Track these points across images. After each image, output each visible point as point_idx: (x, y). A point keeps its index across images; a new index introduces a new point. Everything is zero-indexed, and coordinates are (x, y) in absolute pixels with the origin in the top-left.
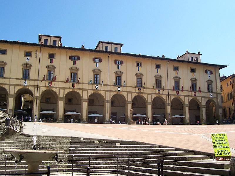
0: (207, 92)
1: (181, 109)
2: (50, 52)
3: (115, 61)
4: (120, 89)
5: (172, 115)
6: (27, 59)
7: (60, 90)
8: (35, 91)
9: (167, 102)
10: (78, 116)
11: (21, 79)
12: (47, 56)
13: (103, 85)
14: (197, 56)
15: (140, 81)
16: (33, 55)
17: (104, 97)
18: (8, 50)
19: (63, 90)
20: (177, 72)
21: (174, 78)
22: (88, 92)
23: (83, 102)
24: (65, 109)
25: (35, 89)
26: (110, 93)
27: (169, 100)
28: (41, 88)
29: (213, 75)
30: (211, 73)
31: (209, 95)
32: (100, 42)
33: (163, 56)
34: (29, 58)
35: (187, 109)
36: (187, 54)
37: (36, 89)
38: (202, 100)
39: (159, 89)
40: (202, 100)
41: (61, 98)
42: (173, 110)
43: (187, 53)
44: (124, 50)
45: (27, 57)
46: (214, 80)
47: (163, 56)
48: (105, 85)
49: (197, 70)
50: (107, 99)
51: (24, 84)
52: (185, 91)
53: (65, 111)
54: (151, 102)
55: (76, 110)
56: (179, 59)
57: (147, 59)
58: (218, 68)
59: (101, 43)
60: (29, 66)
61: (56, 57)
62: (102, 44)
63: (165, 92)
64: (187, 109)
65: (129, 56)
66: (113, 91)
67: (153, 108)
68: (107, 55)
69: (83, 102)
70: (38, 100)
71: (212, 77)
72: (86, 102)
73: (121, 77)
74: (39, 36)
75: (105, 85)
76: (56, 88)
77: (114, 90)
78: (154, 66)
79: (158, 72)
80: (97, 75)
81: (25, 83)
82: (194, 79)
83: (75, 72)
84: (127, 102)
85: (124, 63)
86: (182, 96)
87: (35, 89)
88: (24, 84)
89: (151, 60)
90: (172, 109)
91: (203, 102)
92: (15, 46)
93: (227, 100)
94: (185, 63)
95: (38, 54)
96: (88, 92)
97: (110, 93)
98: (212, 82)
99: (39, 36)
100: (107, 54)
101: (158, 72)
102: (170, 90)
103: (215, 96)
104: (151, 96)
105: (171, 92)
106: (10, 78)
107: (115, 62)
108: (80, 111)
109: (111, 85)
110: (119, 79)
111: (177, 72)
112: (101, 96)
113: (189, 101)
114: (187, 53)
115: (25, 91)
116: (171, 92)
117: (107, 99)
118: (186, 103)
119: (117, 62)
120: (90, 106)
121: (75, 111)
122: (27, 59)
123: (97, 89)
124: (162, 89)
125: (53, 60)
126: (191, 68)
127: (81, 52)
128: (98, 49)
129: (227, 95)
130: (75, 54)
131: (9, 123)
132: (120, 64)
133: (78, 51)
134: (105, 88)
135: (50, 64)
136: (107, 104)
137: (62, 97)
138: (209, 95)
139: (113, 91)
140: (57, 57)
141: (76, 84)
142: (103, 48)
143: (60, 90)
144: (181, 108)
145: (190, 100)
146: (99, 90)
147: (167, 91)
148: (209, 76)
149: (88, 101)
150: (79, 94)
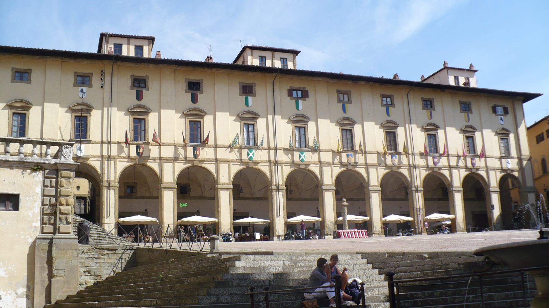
3: (288, 90)
4: (304, 157)
5: (428, 213)
6: (82, 91)
10: (314, 224)
12: (129, 82)
14: (467, 74)
15: (349, 136)
16: (96, 81)
18: (94, 75)
20: (431, 112)
24: (234, 210)
26: (282, 167)
29: (510, 117)
30: (506, 112)
32: (245, 48)
33: (396, 76)
34: (85, 89)
35: (458, 199)
36: (446, 70)
40: (368, 173)
43: (446, 68)
44: (302, 63)
45: (80, 88)
53: (237, 216)
54: (330, 183)
55: (198, 211)
56: (426, 82)
57: (363, 83)
59: (248, 51)
60: (87, 110)
61: (150, 84)
62: (252, 52)
64: (458, 199)
65: (321, 79)
67: (288, 198)
68: (270, 77)
72: (227, 189)
73: (304, 127)
74: (102, 36)
79: (388, 114)
84: (219, 186)
85: (311, 94)
90: (426, 199)
92: (50, 61)
93: (541, 174)
95: (107, 79)
97: (282, 167)
99: (102, 36)
107: (290, 94)
108: (157, 212)
111: (431, 112)
112: (260, 173)
113: (380, 179)
114: (446, 68)
119: (294, 93)
121: (145, 214)
122: (82, 91)
124: (478, 156)
125: (199, 94)
128: (240, 63)
129: (540, 161)
130: (194, 77)
131: (149, 250)
132: (300, 98)
133: (201, 69)
135: (192, 105)
137: (171, 180)
140: (205, 87)
142: (253, 61)
145: (423, 177)
148: (501, 119)
150: (210, 173)
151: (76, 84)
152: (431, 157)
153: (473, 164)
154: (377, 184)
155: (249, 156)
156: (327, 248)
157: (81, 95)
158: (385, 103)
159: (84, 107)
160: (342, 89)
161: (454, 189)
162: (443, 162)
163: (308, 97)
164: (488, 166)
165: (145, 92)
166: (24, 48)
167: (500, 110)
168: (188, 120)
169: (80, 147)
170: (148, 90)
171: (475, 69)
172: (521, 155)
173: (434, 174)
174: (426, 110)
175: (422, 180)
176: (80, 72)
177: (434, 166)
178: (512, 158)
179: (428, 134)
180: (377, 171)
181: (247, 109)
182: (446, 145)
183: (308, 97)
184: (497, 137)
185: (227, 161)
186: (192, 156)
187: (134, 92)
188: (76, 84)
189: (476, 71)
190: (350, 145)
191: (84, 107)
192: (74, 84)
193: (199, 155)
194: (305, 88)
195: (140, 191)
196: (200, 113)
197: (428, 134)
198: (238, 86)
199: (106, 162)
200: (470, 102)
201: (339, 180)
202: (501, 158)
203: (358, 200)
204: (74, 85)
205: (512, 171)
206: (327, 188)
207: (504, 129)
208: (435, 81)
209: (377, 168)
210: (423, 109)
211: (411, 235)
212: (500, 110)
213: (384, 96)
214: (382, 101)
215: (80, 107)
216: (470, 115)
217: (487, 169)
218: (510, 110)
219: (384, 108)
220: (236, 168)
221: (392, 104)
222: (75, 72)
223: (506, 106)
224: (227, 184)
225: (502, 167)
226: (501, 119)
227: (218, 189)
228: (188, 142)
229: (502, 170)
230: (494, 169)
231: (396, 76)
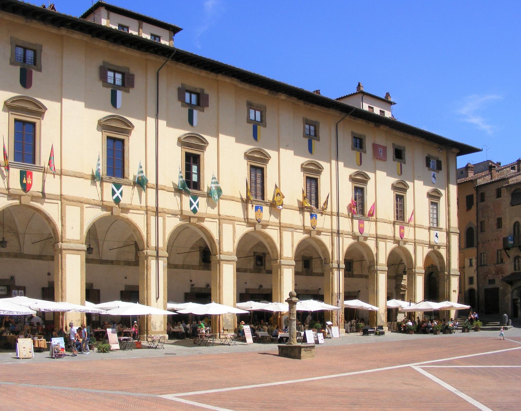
1: (128, 263)
3: (179, 89)
17: (144, 234)
20: (361, 154)
22: (423, 248)
26: (164, 219)
27: (158, 234)
30: (439, 168)
32: (99, 5)
47: (388, 95)
49: (408, 155)
50: (153, 244)
57: (283, 97)
58: (453, 153)
65: (419, 139)
70: (161, 262)
84: (64, 245)
85: (212, 100)
94: (382, 127)
96: (423, 248)
97: (164, 219)
100: (152, 57)
103: (442, 239)
104: (293, 236)
111: (361, 154)
120: (91, 265)
126: (393, 145)
127: (54, 30)
128: (90, 20)
139: (93, 204)
144: (131, 257)
145: (169, 230)
148: (434, 176)
149: (235, 258)
150: (48, 219)
152: (358, 221)
153: (402, 235)
154: (78, 238)
155: (192, 208)
156: (495, 334)
158: (308, 132)
160: (256, 101)
161: (283, 262)
162: (369, 228)
163: (133, 86)
165: (35, 74)
166: (213, 61)
167: (433, 163)
168: (13, 117)
171: (391, 100)
172: (449, 227)
173: (255, 235)
174: (396, 162)
177: (360, 234)
179: (108, 138)
180: (293, 236)
182: (413, 213)
183: (133, 86)
184: (180, 148)
185: (80, 202)
186: (19, 187)
189: (391, 103)
190: (259, 193)
193: (30, 186)
194: (129, 69)
195: (316, 268)
196: (34, 108)
197: (108, 138)
198: (392, 149)
199: (336, 237)
200: (265, 107)
201: (93, 235)
202: (430, 229)
203: (176, 267)
205: (439, 247)
208: (347, 102)
209: (292, 232)
210: (353, 149)
212: (433, 163)
213: (250, 106)
214: (304, 128)
216: (363, 154)
217: (415, 243)
218: (444, 166)
219: (306, 140)
221: (263, 122)
223: (440, 159)
224: (76, 242)
225: (304, 226)
226: (434, 176)
227: (377, 270)
228: (11, 159)
229: (431, 246)
230: (422, 243)
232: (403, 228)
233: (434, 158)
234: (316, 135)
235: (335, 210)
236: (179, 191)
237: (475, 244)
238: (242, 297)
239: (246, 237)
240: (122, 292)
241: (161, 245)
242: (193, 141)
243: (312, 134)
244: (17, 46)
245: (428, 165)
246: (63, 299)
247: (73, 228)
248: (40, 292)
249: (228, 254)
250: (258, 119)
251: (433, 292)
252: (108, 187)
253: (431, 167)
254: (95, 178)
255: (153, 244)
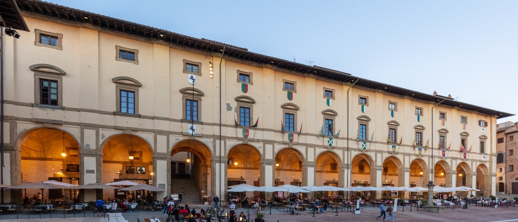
0: (480, 154)
2: (241, 70)
7: (266, 145)
8: (214, 147)
9: (215, 150)
11: (182, 121)
13: (303, 134)
19: (272, 145)
21: (359, 119)
22: (315, 149)
23: (158, 161)
25: (214, 142)
28: (170, 135)
31: (481, 157)
33: (450, 95)
34: (195, 77)
37: (218, 141)
38: (472, 164)
39: (394, 145)
40: (472, 164)
41: (268, 160)
42: (317, 173)
46: (489, 136)
48: (343, 139)
49: (469, 120)
50: (218, 154)
51: (190, 132)
52: (226, 126)
58: (219, 57)
60: (198, 95)
63: (429, 152)
66: (279, 143)
69: (158, 161)
70: (349, 170)
71: (486, 131)
75: (343, 139)
76: (258, 141)
77: (321, 144)
78: (322, 92)
79: (419, 120)
80: (128, 91)
81: (192, 128)
82: (465, 133)
83: (394, 127)
86: (373, 151)
87: (214, 142)
88: (190, 132)
89: (99, 32)
91: (474, 168)
96: (315, 149)
98: (485, 137)
101: (419, 120)
102: (351, 139)
103: (487, 158)
105: (353, 145)
106: (153, 118)
109: (436, 149)
110: (192, 106)
113: (316, 157)
115: (192, 146)
116: (353, 145)
117: (346, 162)
118: (378, 165)
123: (330, 145)
134: (342, 144)
136: (346, 170)
137: (93, 147)
138: (481, 157)
139: (279, 143)
141: (397, 146)
143: (266, 145)
145: (353, 157)
146: (333, 148)
147: (431, 150)
149: (383, 168)
151: (185, 71)
157: (482, 131)
159: (195, 92)
164: (222, 135)
165: (249, 86)
169: (192, 127)
170: (368, 106)
175: (227, 152)
176: (42, 30)
178: (487, 154)
181: (328, 108)
187: (240, 85)
188: (185, 71)
191: (195, 92)
192: (116, 57)
204: (184, 72)
206: (378, 168)
207: (484, 136)
211: (150, 210)
213: (390, 103)
215: (192, 92)
218: (489, 125)
220: (386, 155)
221: (396, 109)
222: (184, 60)
231: (450, 95)
232: (293, 135)
233: (483, 121)
234: (421, 113)
235: (430, 146)
236: (358, 140)
237: (504, 161)
238: (384, 185)
239: (322, 154)
240: (254, 182)
241: (349, 163)
242: (443, 131)
243: (419, 113)
244: (187, 64)
245: (480, 124)
246: (264, 185)
247: (311, 156)
248: (253, 183)
249: (379, 166)
250: (393, 108)
251: (463, 181)
252: (417, 149)
253: (482, 125)
254: (414, 147)
255: (431, 168)
